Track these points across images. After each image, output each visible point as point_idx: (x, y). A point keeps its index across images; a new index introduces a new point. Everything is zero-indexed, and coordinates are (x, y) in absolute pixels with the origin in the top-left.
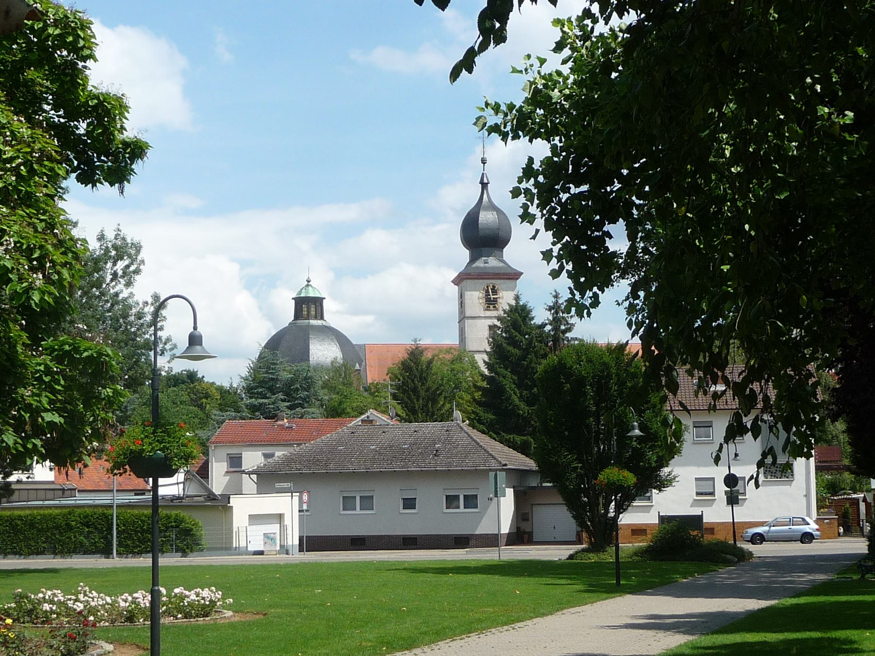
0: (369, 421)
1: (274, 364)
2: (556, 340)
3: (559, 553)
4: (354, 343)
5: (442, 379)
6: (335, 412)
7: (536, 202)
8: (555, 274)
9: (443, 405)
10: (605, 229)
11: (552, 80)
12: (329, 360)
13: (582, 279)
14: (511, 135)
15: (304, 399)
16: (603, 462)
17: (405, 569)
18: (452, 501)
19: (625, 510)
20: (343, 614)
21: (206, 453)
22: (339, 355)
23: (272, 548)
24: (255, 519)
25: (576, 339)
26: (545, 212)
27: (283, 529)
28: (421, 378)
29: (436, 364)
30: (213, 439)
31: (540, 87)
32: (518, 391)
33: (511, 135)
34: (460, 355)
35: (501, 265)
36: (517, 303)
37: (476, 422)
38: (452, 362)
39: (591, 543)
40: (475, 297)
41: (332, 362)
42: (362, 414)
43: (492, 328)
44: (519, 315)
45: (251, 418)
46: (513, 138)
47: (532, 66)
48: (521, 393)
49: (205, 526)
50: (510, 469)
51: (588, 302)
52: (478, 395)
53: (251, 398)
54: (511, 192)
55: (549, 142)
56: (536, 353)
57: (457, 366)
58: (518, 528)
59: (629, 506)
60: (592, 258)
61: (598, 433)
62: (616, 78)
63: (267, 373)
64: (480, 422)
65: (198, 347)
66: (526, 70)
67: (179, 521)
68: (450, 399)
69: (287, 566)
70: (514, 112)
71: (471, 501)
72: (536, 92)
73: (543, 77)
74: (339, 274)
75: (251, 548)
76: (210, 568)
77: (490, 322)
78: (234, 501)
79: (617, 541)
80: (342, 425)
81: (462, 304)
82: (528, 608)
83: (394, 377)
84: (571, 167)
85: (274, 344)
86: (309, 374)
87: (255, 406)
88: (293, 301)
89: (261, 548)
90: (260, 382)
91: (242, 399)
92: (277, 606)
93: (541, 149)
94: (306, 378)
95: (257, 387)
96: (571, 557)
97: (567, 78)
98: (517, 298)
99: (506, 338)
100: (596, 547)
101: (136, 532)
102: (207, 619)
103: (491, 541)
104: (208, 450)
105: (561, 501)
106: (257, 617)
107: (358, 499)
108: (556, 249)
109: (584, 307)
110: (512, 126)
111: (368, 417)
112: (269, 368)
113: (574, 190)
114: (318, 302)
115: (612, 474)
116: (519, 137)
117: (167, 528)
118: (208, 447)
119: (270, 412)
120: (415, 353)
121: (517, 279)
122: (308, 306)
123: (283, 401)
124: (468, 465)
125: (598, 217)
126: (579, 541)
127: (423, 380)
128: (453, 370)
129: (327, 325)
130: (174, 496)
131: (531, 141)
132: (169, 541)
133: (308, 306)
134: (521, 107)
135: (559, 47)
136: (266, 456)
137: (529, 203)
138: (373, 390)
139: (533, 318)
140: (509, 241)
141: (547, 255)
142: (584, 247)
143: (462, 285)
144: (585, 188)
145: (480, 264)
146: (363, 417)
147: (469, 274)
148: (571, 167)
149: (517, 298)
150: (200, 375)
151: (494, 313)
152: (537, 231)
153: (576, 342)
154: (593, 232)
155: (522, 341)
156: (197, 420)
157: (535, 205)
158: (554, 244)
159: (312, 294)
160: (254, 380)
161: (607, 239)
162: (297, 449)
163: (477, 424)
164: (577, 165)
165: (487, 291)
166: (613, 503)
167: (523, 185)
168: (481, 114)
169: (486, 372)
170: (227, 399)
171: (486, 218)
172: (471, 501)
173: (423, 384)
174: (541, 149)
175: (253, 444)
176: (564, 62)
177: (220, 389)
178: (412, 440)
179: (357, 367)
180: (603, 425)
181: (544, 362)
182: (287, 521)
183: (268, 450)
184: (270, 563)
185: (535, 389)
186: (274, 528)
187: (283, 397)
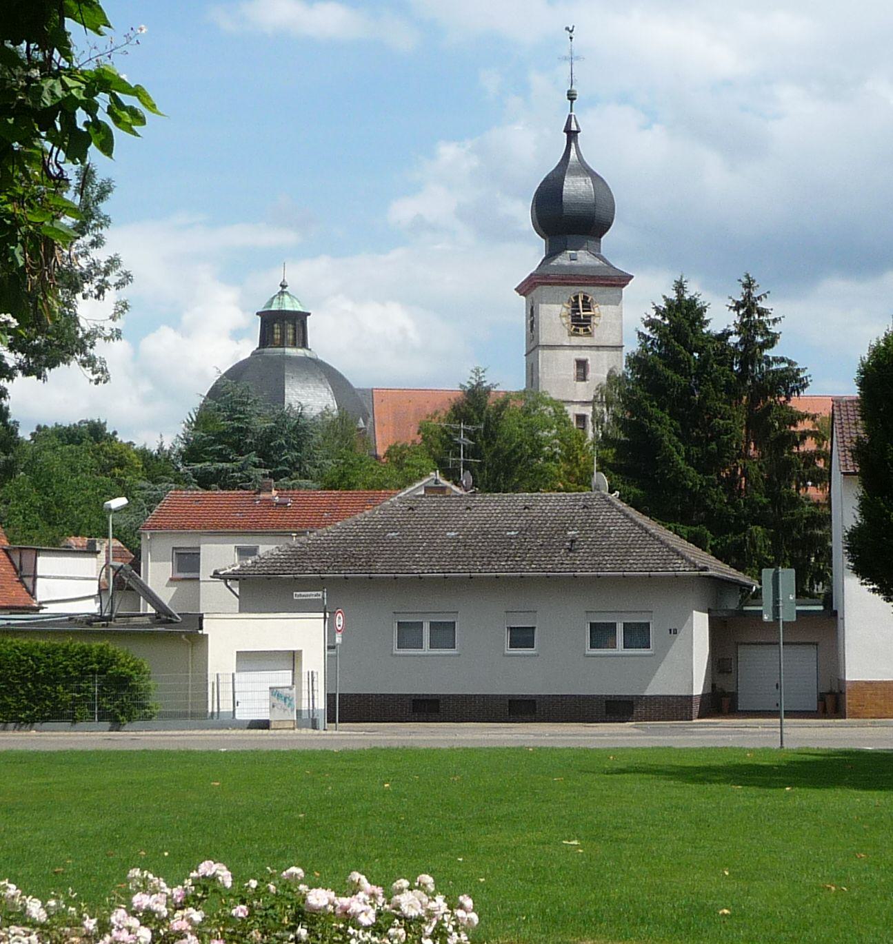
1: (243, 404)
4: (355, 386)
15: (292, 465)
18: (601, 634)
22: (333, 405)
24: (249, 660)
25: (782, 360)
32: (683, 448)
35: (598, 262)
36: (680, 296)
40: (554, 314)
49: (155, 669)
50: (710, 577)
63: (230, 418)
67: (106, 661)
71: (638, 635)
75: (243, 715)
81: (533, 325)
88: (259, 318)
89: (264, 716)
94: (295, 429)
101: (24, 680)
103: (674, 708)
107: (426, 627)
114: (298, 320)
117: (84, 674)
121: (624, 286)
122: (281, 326)
130: (93, 615)
132: (86, 698)
133: (281, 326)
136: (243, 552)
140: (609, 225)
143: (534, 293)
145: (563, 260)
147: (547, 276)
149: (680, 287)
150: (109, 430)
159: (289, 305)
165: (575, 305)
170: (153, 465)
171: (575, 187)
172: (638, 635)
175: (220, 530)
177: (144, 454)
179: (361, 424)
183: (247, 542)
186: (282, 678)
187: (256, 460)
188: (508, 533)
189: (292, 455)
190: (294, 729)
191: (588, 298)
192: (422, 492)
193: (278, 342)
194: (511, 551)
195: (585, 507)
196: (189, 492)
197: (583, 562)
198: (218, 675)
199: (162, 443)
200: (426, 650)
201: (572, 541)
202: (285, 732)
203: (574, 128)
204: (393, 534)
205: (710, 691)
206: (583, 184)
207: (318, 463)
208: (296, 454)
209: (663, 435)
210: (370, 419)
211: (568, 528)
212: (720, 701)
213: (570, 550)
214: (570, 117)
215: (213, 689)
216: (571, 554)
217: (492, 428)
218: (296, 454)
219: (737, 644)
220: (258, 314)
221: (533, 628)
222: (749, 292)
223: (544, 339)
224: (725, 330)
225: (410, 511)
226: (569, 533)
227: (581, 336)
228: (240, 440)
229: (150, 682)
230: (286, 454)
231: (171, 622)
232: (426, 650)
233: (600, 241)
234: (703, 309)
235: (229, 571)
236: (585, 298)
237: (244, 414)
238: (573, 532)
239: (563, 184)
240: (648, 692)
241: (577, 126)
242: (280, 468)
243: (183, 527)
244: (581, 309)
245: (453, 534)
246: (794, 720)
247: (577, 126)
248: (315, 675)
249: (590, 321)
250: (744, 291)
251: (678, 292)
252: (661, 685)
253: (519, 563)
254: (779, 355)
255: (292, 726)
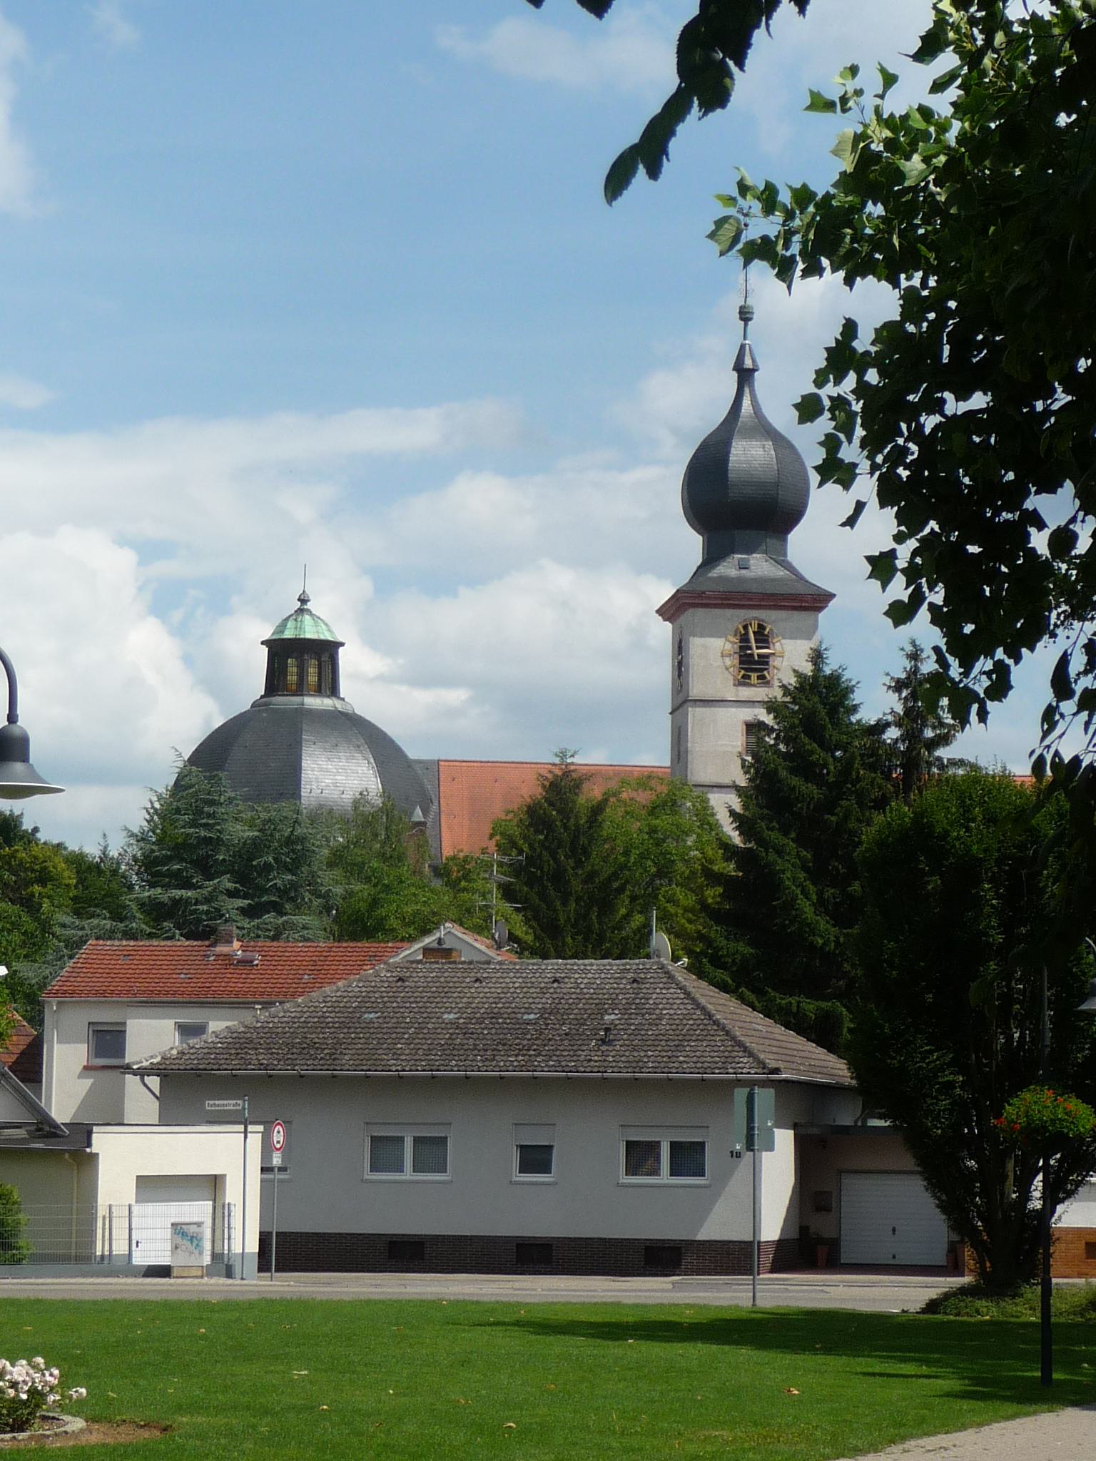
0: (441, 952)
1: (212, 803)
2: (912, 763)
3: (902, 1295)
5: (626, 853)
6: (361, 926)
7: (860, 432)
8: (901, 613)
9: (627, 917)
10: (1029, 504)
11: (909, 130)
12: (348, 797)
13: (969, 628)
14: (801, 266)
16: (1020, 1072)
17: (517, 1323)
18: (640, 1156)
19: (1070, 1194)
20: (360, 1434)
21: (36, 1020)
23: (192, 1261)
24: (153, 1187)
26: (879, 459)
27: (221, 1213)
28: (573, 850)
29: (612, 814)
30: (55, 984)
31: (877, 147)
32: (812, 889)
33: (801, 266)
34: (672, 794)
35: (781, 573)
36: (817, 669)
37: (705, 962)
38: (653, 810)
39: (982, 1273)
40: (714, 652)
41: (356, 803)
42: (425, 932)
43: (754, 728)
44: (823, 696)
45: (151, 936)
46: (806, 273)
47: (859, 93)
48: (820, 894)
50: (786, 1081)
51: (981, 686)
52: (712, 894)
53: (152, 885)
54: (796, 406)
55: (895, 284)
56: (860, 796)
57: (663, 822)
58: (804, 1230)
59: (1078, 1184)
60: (994, 577)
61: (1008, 999)
62: (1069, 125)
63: (193, 824)
64: (717, 961)
65: (18, 767)
66: (844, 100)
68: (645, 902)
69: (228, 1306)
70: (811, 209)
71: (688, 1158)
72: (866, 159)
73: (889, 123)
74: (385, 583)
75: (140, 1259)
76: (35, 1305)
77: (748, 714)
78: (104, 1142)
79: (1047, 1268)
80: (376, 958)
81: (680, 668)
82: (818, 1433)
83: (508, 845)
84: (947, 349)
85: (214, 753)
86: (299, 831)
87: (162, 904)
88: (265, 649)
89: (165, 1260)
90: (176, 847)
91: (130, 887)
92: (193, 1407)
93: (877, 303)
94: (289, 841)
95: (167, 860)
96: (932, 1306)
97: (943, 128)
98: (817, 657)
99: (785, 756)
100: (995, 1284)
102: (21, 1436)
103: (734, 1258)
104: (41, 1012)
105: (909, 1162)
106: (146, 1434)
108: (904, 552)
109: (974, 696)
110: (804, 243)
111: (440, 941)
112: (199, 812)
113: (953, 406)
114: (326, 652)
115: (1037, 1104)
116: (819, 271)
118: (41, 1005)
119: (199, 921)
120: (561, 787)
121: (820, 609)
122: (300, 662)
123: (232, 894)
124: (685, 1067)
125: (1011, 476)
126: (954, 1267)
127: (580, 852)
128: (653, 831)
129: (347, 709)
131: (849, 281)
133: (300, 662)
134: (828, 197)
135: (930, 46)
136: (186, 1030)
137: (842, 436)
138: (455, 875)
139: (855, 709)
141: (882, 566)
142: (973, 549)
144: (979, 401)
145: (727, 569)
146: (428, 940)
147: (701, 594)
148: (947, 349)
149: (817, 657)
151: (760, 693)
152: (860, 506)
153: (961, 772)
154: (997, 513)
155: (825, 766)
156: (16, 937)
157: (856, 441)
158: (899, 538)
159: (310, 631)
160: (160, 841)
161: (1033, 530)
162: (263, 1015)
163: (708, 967)
164: (962, 343)
166: (1040, 1177)
167: (830, 390)
168: (732, 211)
169: (736, 838)
170: (92, 884)
171: (748, 456)
172: (688, 1158)
173: (579, 864)
174: (877, 303)
175: (155, 999)
176: (939, 86)
177: (78, 862)
178: (547, 1001)
180: (1019, 981)
181: (879, 818)
182: (232, 1194)
183: (191, 1016)
184: (184, 1297)
185: (856, 887)
186: (198, 1211)
187: (230, 886)
188: (526, 1017)
189: (282, 879)
190: (202, 1277)
191: (764, 628)
192: (421, 957)
193: (294, 687)
194: (525, 1042)
195: (635, 981)
196: (117, 943)
197: (618, 1058)
198: (110, 1206)
199: (106, 847)
200: (408, 1174)
201: (607, 1030)
202: (188, 1281)
203: (748, 363)
204: (372, 1016)
205: (796, 1235)
206: (760, 451)
207: (323, 889)
208: (289, 877)
209: (783, 872)
210: (434, 807)
211: (606, 1010)
212: (807, 1248)
213: (603, 1041)
214: (743, 347)
215: (104, 1224)
216: (604, 1048)
217: (583, 840)
218: (289, 877)
219: (840, 1172)
220: (812, 92)
221: (551, 1147)
222: (916, 666)
223: (697, 689)
224: (880, 720)
225: (400, 984)
226: (607, 1017)
227: (754, 685)
228: (208, 856)
229: (21, 1216)
230: (275, 878)
231: (54, 1135)
232: (408, 1174)
233: (785, 540)
234: (850, 690)
235: (145, 1064)
236: (761, 627)
237: (214, 817)
238: (613, 1017)
239: (729, 452)
240: (702, 1236)
241: (754, 361)
242: (265, 898)
243: (103, 994)
244: (754, 645)
245: (452, 1016)
246: (886, 1277)
247: (754, 361)
248: (232, 1208)
249: (767, 663)
250: (908, 665)
251: (815, 664)
252: (718, 1226)
253: (533, 1058)
254: (958, 757)
255: (199, 1273)
